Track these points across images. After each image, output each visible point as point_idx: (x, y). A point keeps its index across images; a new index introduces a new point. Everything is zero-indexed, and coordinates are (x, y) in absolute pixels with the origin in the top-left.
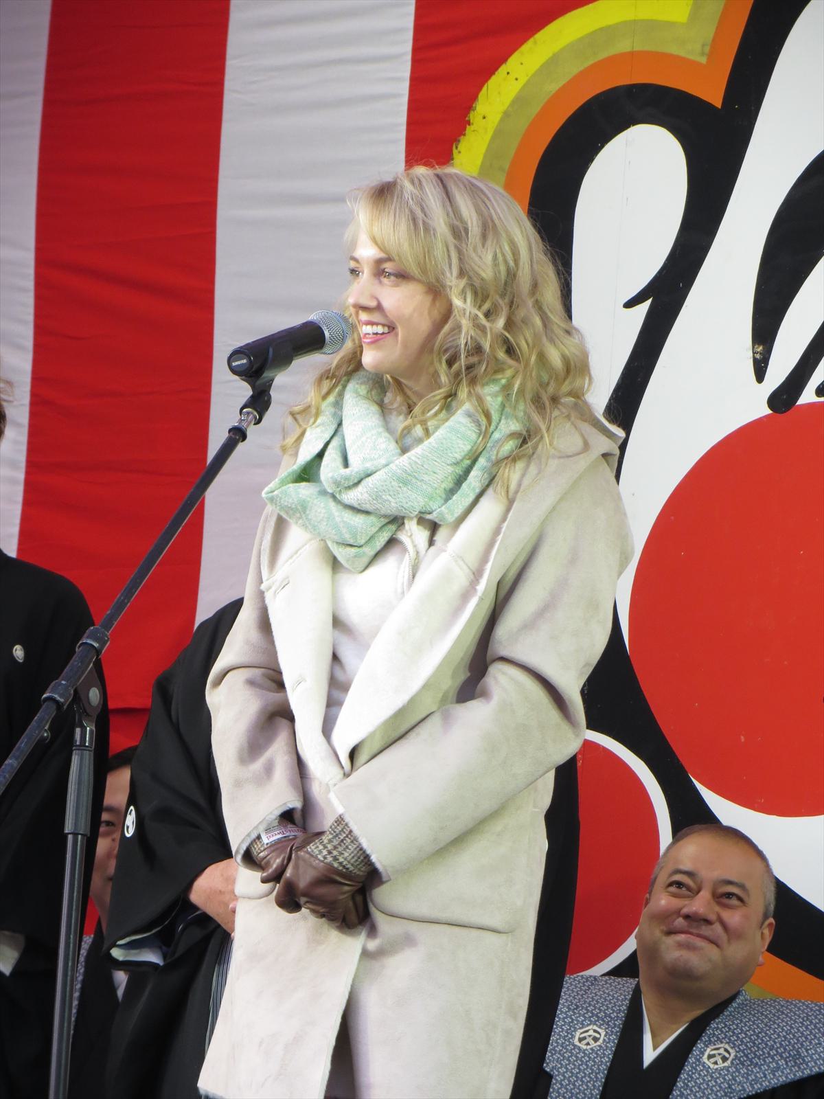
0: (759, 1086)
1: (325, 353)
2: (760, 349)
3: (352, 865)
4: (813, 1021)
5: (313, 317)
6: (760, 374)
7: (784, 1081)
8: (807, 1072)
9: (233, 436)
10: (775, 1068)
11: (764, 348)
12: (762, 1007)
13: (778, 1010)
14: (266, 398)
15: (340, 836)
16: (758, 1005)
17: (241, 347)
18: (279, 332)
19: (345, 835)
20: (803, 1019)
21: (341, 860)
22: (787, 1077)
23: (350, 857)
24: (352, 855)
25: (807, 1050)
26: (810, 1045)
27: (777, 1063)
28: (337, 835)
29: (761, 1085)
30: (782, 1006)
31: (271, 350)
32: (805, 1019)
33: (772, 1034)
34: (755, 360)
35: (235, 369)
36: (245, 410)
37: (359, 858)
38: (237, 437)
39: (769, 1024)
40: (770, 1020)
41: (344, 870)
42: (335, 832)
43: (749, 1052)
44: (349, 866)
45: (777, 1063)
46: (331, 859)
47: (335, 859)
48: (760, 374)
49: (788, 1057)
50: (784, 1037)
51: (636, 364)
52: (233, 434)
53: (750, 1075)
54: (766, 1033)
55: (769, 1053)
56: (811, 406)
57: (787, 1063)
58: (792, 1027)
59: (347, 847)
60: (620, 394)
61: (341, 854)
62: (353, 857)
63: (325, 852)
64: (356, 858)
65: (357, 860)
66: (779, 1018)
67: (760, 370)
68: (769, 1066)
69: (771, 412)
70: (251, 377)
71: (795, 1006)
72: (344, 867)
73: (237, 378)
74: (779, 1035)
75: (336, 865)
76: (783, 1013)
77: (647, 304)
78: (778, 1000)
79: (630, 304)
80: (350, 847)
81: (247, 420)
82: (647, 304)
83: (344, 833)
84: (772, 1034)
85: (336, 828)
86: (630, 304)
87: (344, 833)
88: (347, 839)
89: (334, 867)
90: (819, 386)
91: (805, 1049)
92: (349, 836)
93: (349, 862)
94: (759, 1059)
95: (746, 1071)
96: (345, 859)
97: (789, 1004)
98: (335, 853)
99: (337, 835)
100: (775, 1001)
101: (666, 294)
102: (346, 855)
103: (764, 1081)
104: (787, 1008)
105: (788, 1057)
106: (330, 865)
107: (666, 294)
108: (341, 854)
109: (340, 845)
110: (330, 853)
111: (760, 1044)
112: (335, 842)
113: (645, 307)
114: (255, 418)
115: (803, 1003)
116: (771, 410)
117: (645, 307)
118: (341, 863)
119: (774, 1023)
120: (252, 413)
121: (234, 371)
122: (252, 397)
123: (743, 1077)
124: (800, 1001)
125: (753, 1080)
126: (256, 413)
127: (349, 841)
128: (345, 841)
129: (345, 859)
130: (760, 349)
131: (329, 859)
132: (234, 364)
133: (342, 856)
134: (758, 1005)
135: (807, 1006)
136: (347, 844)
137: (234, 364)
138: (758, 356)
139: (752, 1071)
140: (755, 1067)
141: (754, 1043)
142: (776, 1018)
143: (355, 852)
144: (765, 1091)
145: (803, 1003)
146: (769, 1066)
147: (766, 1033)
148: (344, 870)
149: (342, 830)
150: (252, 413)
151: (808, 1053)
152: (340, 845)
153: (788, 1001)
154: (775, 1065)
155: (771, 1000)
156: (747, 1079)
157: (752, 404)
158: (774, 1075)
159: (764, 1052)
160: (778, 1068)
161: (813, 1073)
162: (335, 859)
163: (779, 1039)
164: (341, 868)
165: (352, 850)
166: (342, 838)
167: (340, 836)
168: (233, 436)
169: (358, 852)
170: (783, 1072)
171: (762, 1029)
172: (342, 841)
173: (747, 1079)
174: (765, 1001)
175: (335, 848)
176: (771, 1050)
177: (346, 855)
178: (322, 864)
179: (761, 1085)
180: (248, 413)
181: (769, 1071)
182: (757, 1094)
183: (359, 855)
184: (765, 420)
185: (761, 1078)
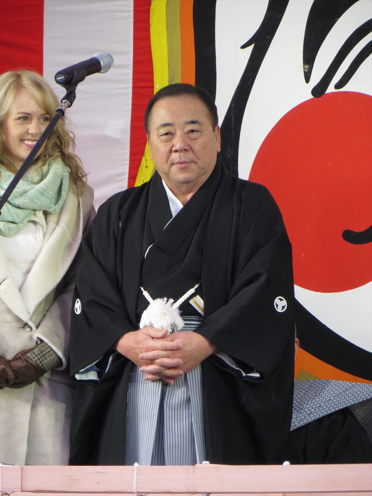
0: (303, 423)
1: (101, 73)
2: (307, 67)
3: (47, 366)
4: (327, 389)
5: (95, 55)
6: (307, 79)
7: (322, 416)
8: (325, 413)
9: (58, 113)
10: (309, 413)
11: (309, 67)
12: (302, 385)
13: (310, 386)
14: (73, 95)
15: (43, 353)
16: (300, 384)
17: (61, 71)
18: (79, 63)
19: (45, 353)
20: (322, 389)
21: (43, 363)
22: (316, 417)
23: (47, 363)
24: (48, 362)
25: (324, 403)
26: (326, 401)
27: (310, 411)
28: (41, 352)
29: (304, 422)
30: (312, 383)
31: (75, 72)
32: (323, 388)
33: (307, 398)
34: (305, 72)
35: (58, 81)
36: (63, 101)
37: (50, 364)
38: (60, 114)
39: (323, 385)
40: (306, 391)
41: (43, 368)
42: (41, 350)
43: (297, 407)
44: (45, 366)
45: (310, 411)
46: (39, 362)
47: (41, 362)
48: (307, 79)
49: (315, 408)
50: (313, 398)
51: (247, 75)
52: (58, 112)
53: (298, 418)
54: (304, 398)
55: (306, 407)
56: (333, 94)
57: (315, 411)
58: (316, 393)
59: (46, 358)
60: (240, 90)
61: (43, 360)
62: (48, 363)
63: (36, 358)
64: (49, 364)
65: (49, 365)
66: (310, 390)
67: (307, 78)
68: (306, 413)
69: (313, 97)
70: (66, 85)
71: (318, 383)
72: (43, 366)
73: (59, 86)
74: (310, 398)
75: (40, 365)
76: (312, 387)
77: (252, 46)
78: (315, 380)
79: (243, 47)
80: (47, 358)
81: (65, 105)
82: (252, 46)
83: (45, 352)
84: (307, 398)
85: (41, 349)
86: (243, 47)
87: (45, 352)
88: (46, 354)
89: (39, 365)
90: (336, 84)
91: (323, 403)
92: (48, 354)
93: (46, 365)
94: (302, 410)
95: (296, 416)
96: (45, 363)
97: (315, 382)
98: (41, 360)
99: (41, 352)
100: (308, 381)
101: (261, 42)
102: (45, 361)
103: (305, 420)
104: (314, 384)
105: (315, 408)
106: (38, 364)
107: (261, 42)
108: (43, 360)
109: (43, 357)
110: (39, 359)
111: (301, 403)
112: (41, 355)
113: (251, 48)
114: (69, 104)
115: (322, 381)
116: (313, 96)
117: (251, 48)
118: (42, 365)
119: (308, 392)
120: (67, 102)
121: (58, 82)
122: (67, 94)
123: (295, 419)
124: (320, 380)
125: (300, 420)
126: (69, 102)
127: (47, 356)
128: (45, 355)
129: (45, 363)
130: (307, 67)
131: (38, 362)
132: (58, 79)
133: (44, 362)
134: (300, 384)
135: (323, 382)
136: (46, 357)
137: (58, 79)
138: (306, 70)
139: (299, 416)
140: (300, 414)
141: (299, 403)
142: (309, 390)
143: (50, 361)
144: (306, 425)
145: (322, 381)
146: (306, 413)
147: (304, 398)
148: (43, 368)
149: (44, 350)
150: (67, 102)
151: (325, 405)
152: (43, 357)
153: (314, 381)
154: (309, 412)
155: (306, 380)
156: (297, 420)
157: (304, 93)
158: (309, 417)
159: (304, 407)
160: (311, 413)
161: (328, 414)
162: (41, 362)
163: (311, 400)
164: (42, 367)
165: (48, 360)
166: (44, 354)
167: (43, 353)
168: (58, 113)
169: (51, 361)
170: (313, 415)
171: (302, 396)
172: (44, 355)
173: (297, 420)
174: (303, 381)
175: (41, 357)
176: (307, 405)
177: (45, 361)
178: (35, 363)
179: (304, 422)
180: (65, 102)
181: (307, 415)
182: (302, 426)
183: (51, 362)
184: (310, 101)
185: (303, 419)
